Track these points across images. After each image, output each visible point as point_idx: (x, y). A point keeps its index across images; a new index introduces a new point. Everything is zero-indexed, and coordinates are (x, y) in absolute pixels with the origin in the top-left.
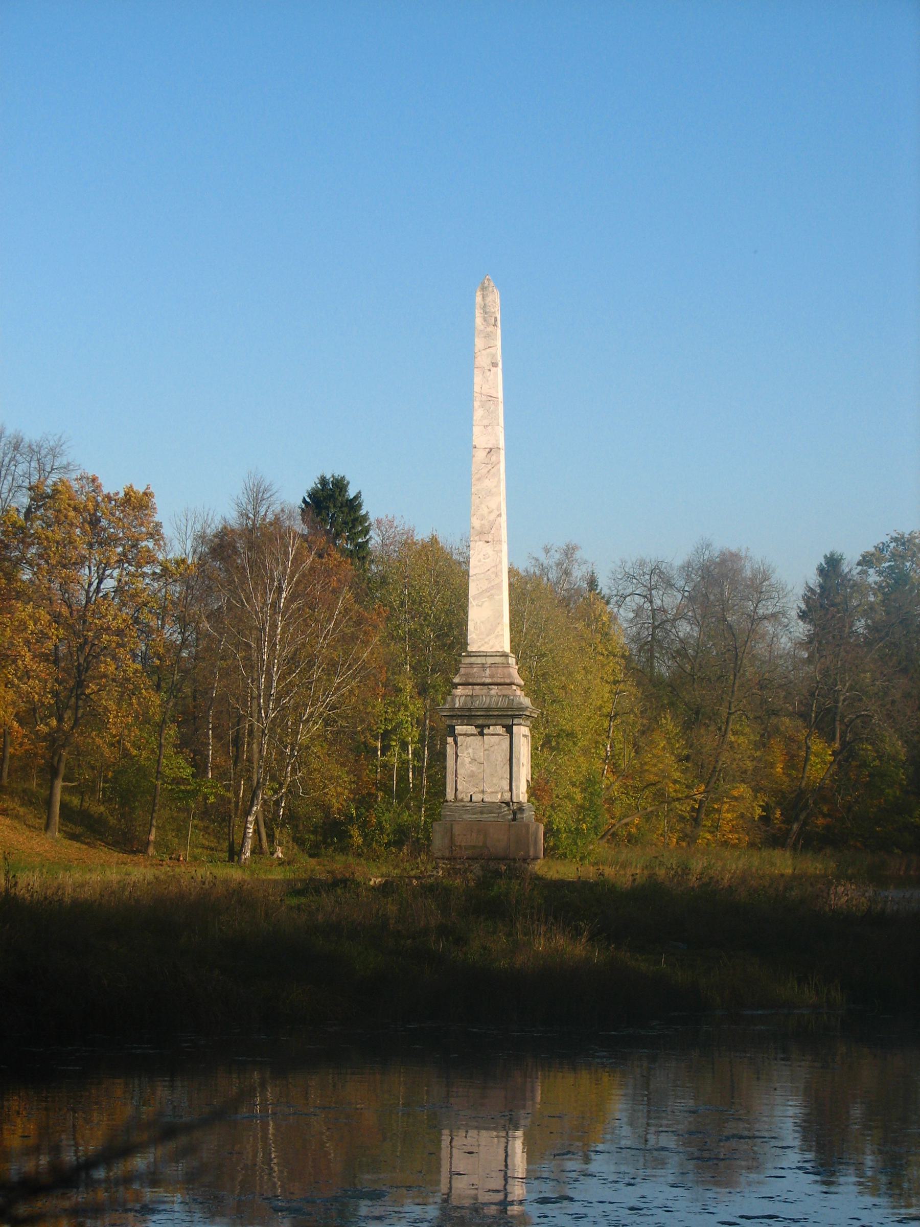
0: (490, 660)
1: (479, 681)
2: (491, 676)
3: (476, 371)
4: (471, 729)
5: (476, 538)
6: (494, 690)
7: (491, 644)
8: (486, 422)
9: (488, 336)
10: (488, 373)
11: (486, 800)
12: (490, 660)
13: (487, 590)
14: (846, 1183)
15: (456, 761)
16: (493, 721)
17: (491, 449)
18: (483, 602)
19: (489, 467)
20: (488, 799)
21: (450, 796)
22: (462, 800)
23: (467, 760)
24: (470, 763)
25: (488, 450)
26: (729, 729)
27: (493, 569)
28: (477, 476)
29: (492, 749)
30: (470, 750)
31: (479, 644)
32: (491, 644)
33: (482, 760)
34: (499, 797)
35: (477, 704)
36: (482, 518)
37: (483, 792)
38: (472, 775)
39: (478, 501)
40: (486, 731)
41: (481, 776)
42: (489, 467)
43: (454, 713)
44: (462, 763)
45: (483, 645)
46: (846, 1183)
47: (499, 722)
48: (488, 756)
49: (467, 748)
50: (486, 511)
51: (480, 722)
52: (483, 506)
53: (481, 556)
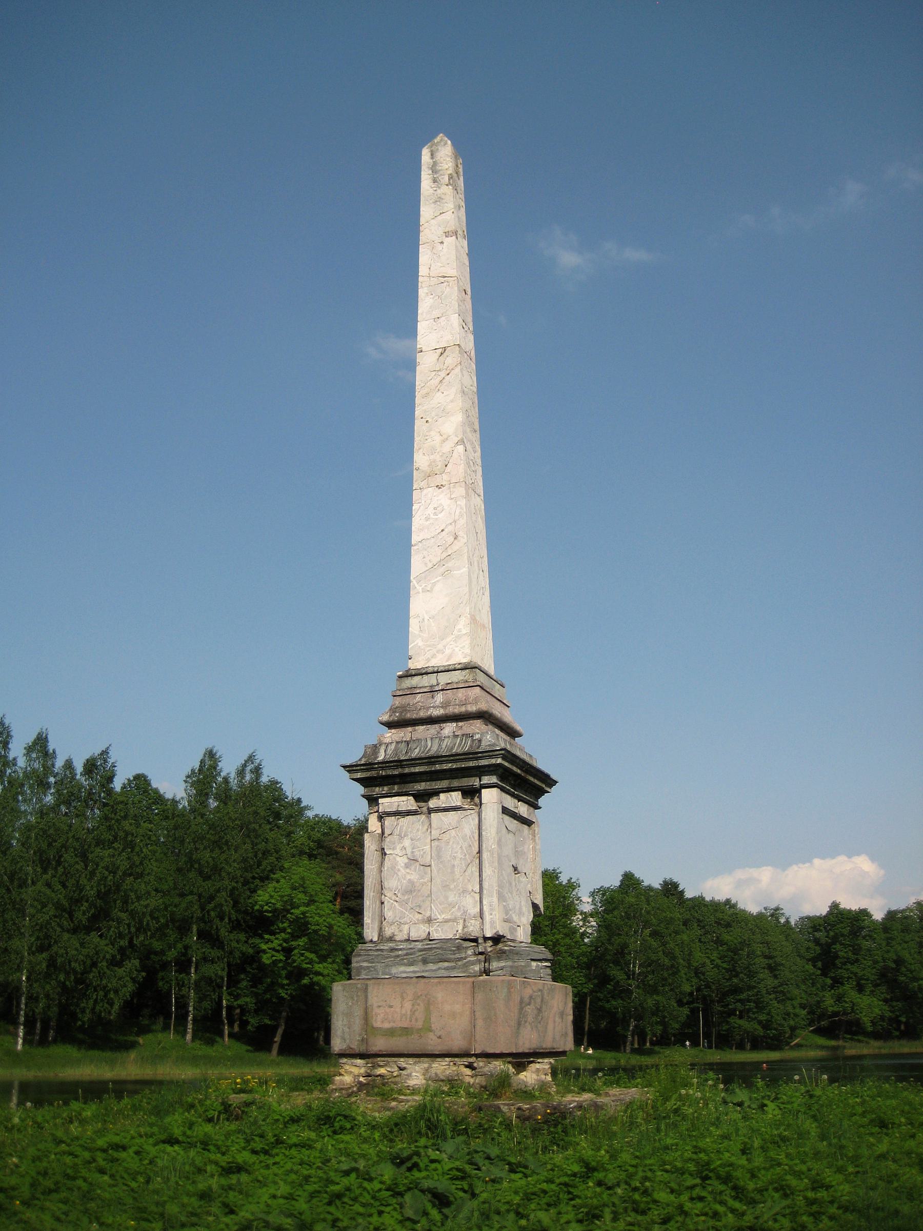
0: (444, 679)
1: (422, 714)
2: (445, 705)
3: (422, 249)
4: (407, 803)
5: (422, 484)
6: (449, 728)
7: (448, 652)
8: (436, 313)
9: (439, 200)
10: (440, 247)
11: (435, 935)
12: (444, 679)
13: (441, 563)
14: (565, 1003)
15: (382, 864)
16: (444, 784)
17: (445, 349)
18: (434, 584)
19: (443, 374)
20: (439, 933)
21: (370, 932)
22: (391, 939)
23: (402, 861)
24: (407, 866)
25: (440, 351)
26: (406, 758)
27: (450, 528)
28: (424, 391)
29: (445, 837)
30: (407, 842)
31: (428, 655)
32: (448, 652)
33: (427, 860)
34: (460, 928)
35: (415, 753)
36: (433, 450)
37: (429, 921)
38: (411, 890)
39: (425, 427)
40: (433, 803)
41: (425, 891)
42: (443, 374)
43: (373, 773)
44: (393, 868)
45: (434, 656)
46: (565, 1003)
47: (456, 783)
48: (439, 849)
49: (401, 837)
50: (438, 439)
51: (422, 786)
52: (433, 433)
53: (430, 511)
